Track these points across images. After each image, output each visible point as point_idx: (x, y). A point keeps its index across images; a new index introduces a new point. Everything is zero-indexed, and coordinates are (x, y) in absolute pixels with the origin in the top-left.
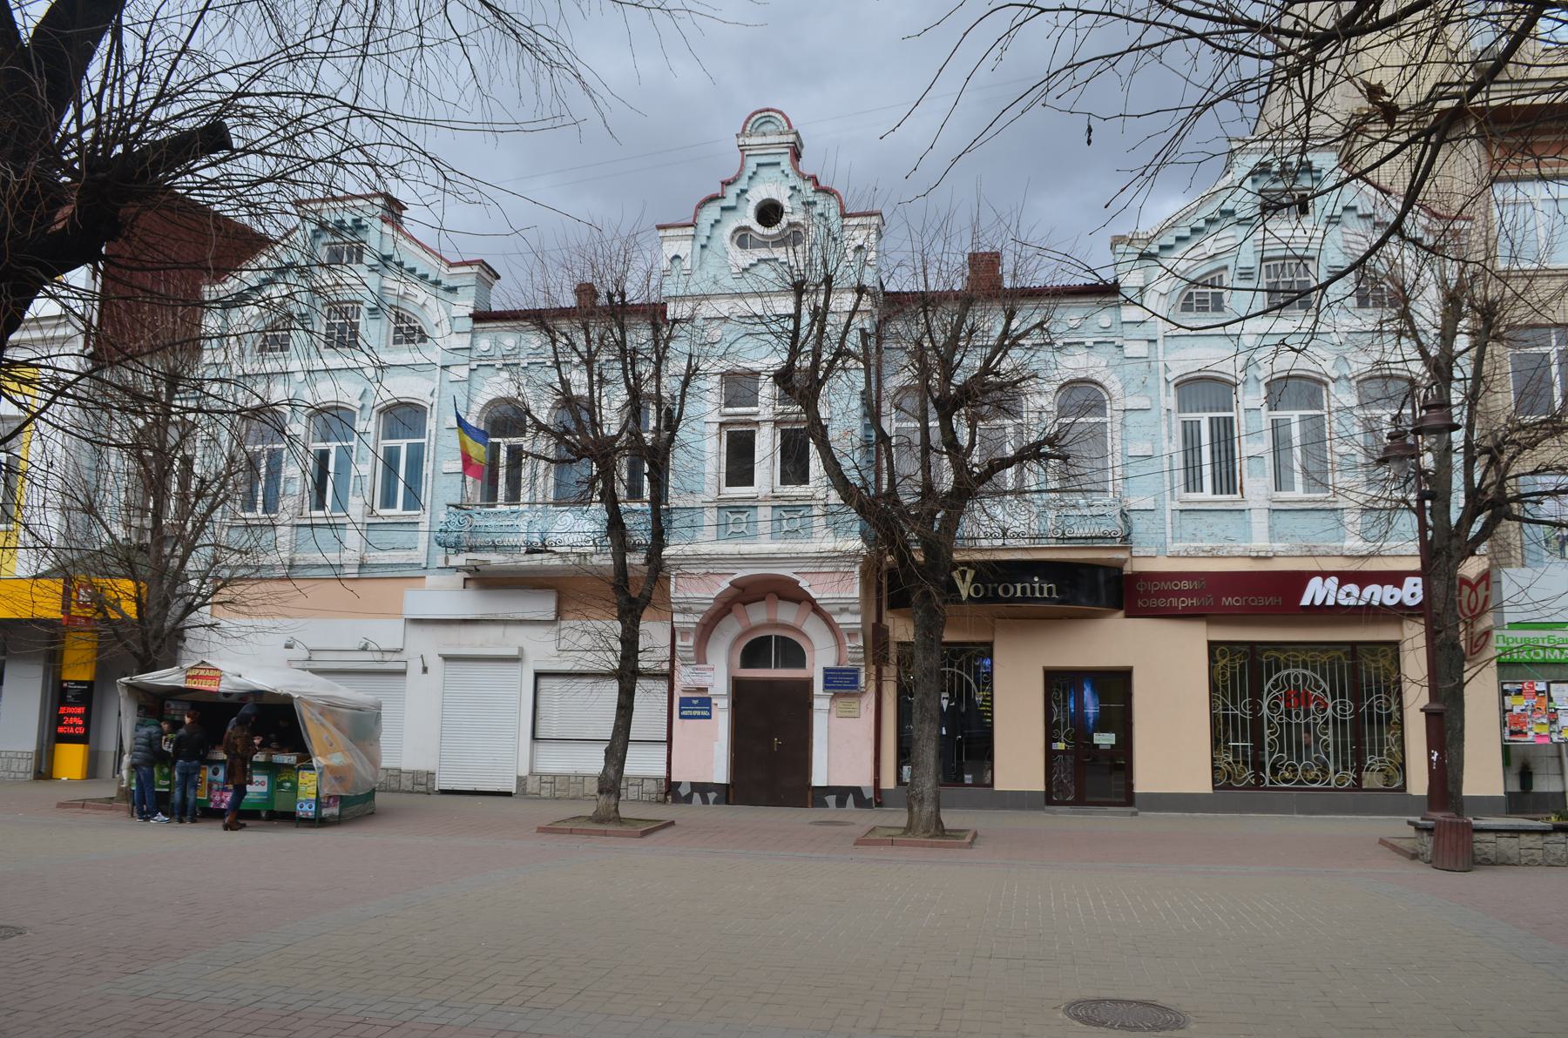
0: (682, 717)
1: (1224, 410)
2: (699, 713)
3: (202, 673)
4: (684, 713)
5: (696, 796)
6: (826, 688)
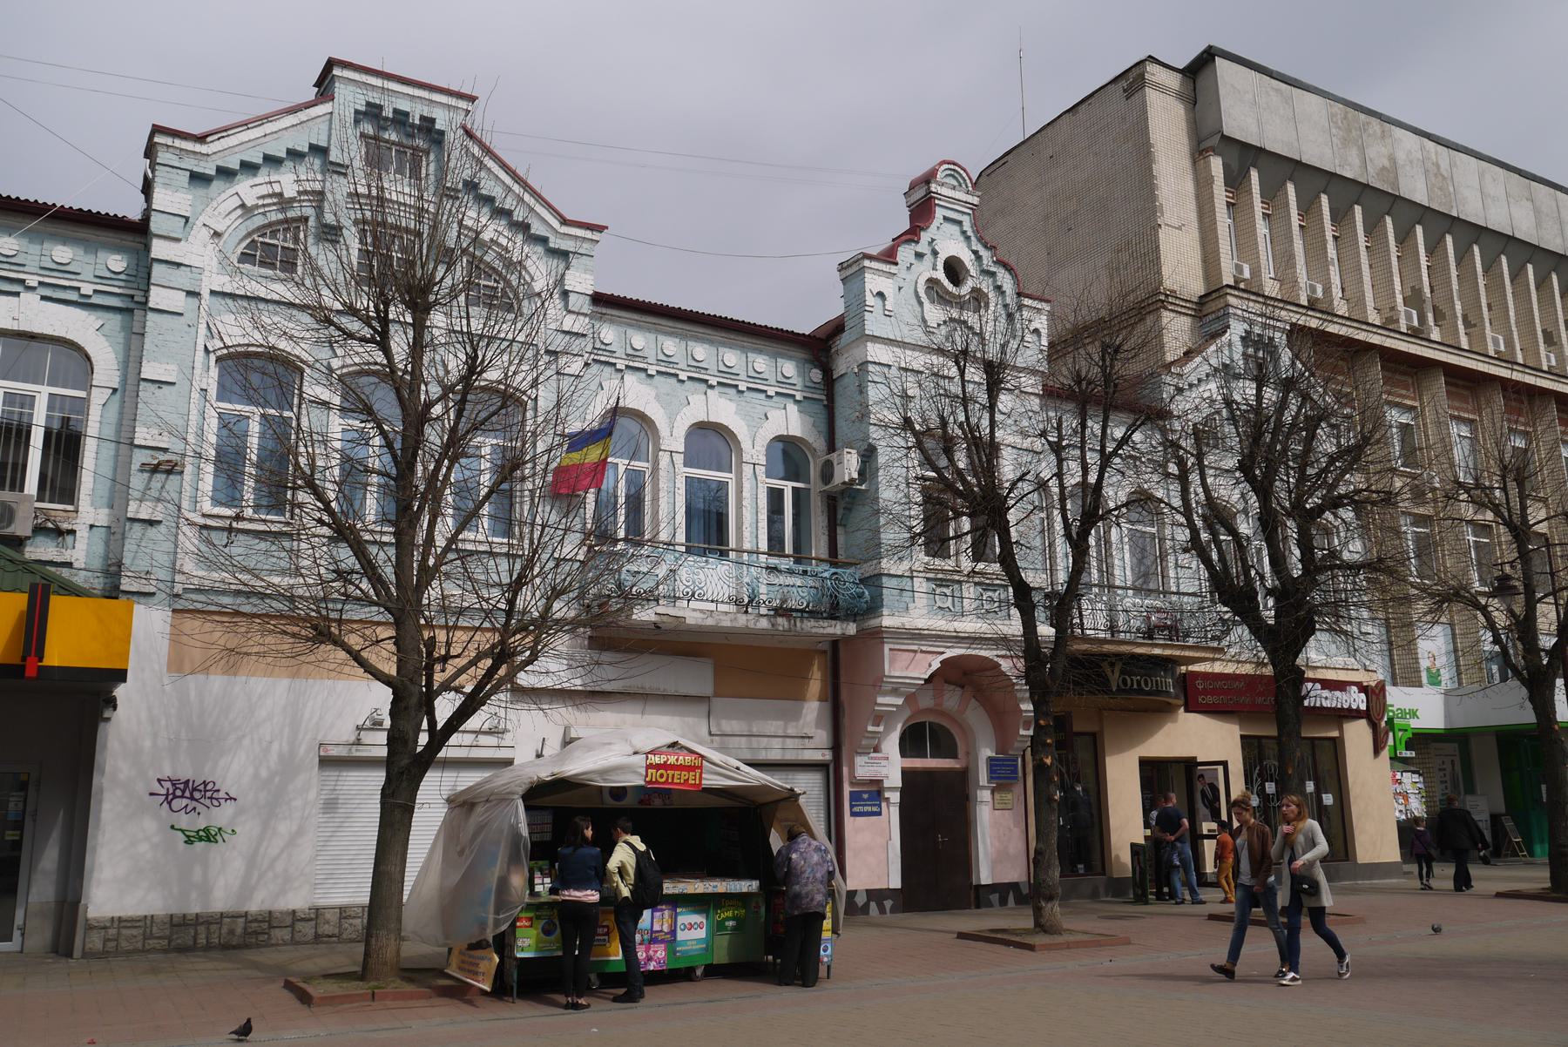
0: (853, 814)
1: (6, 469)
2: (869, 809)
3: (672, 760)
4: (856, 809)
5: (873, 905)
6: (991, 779)
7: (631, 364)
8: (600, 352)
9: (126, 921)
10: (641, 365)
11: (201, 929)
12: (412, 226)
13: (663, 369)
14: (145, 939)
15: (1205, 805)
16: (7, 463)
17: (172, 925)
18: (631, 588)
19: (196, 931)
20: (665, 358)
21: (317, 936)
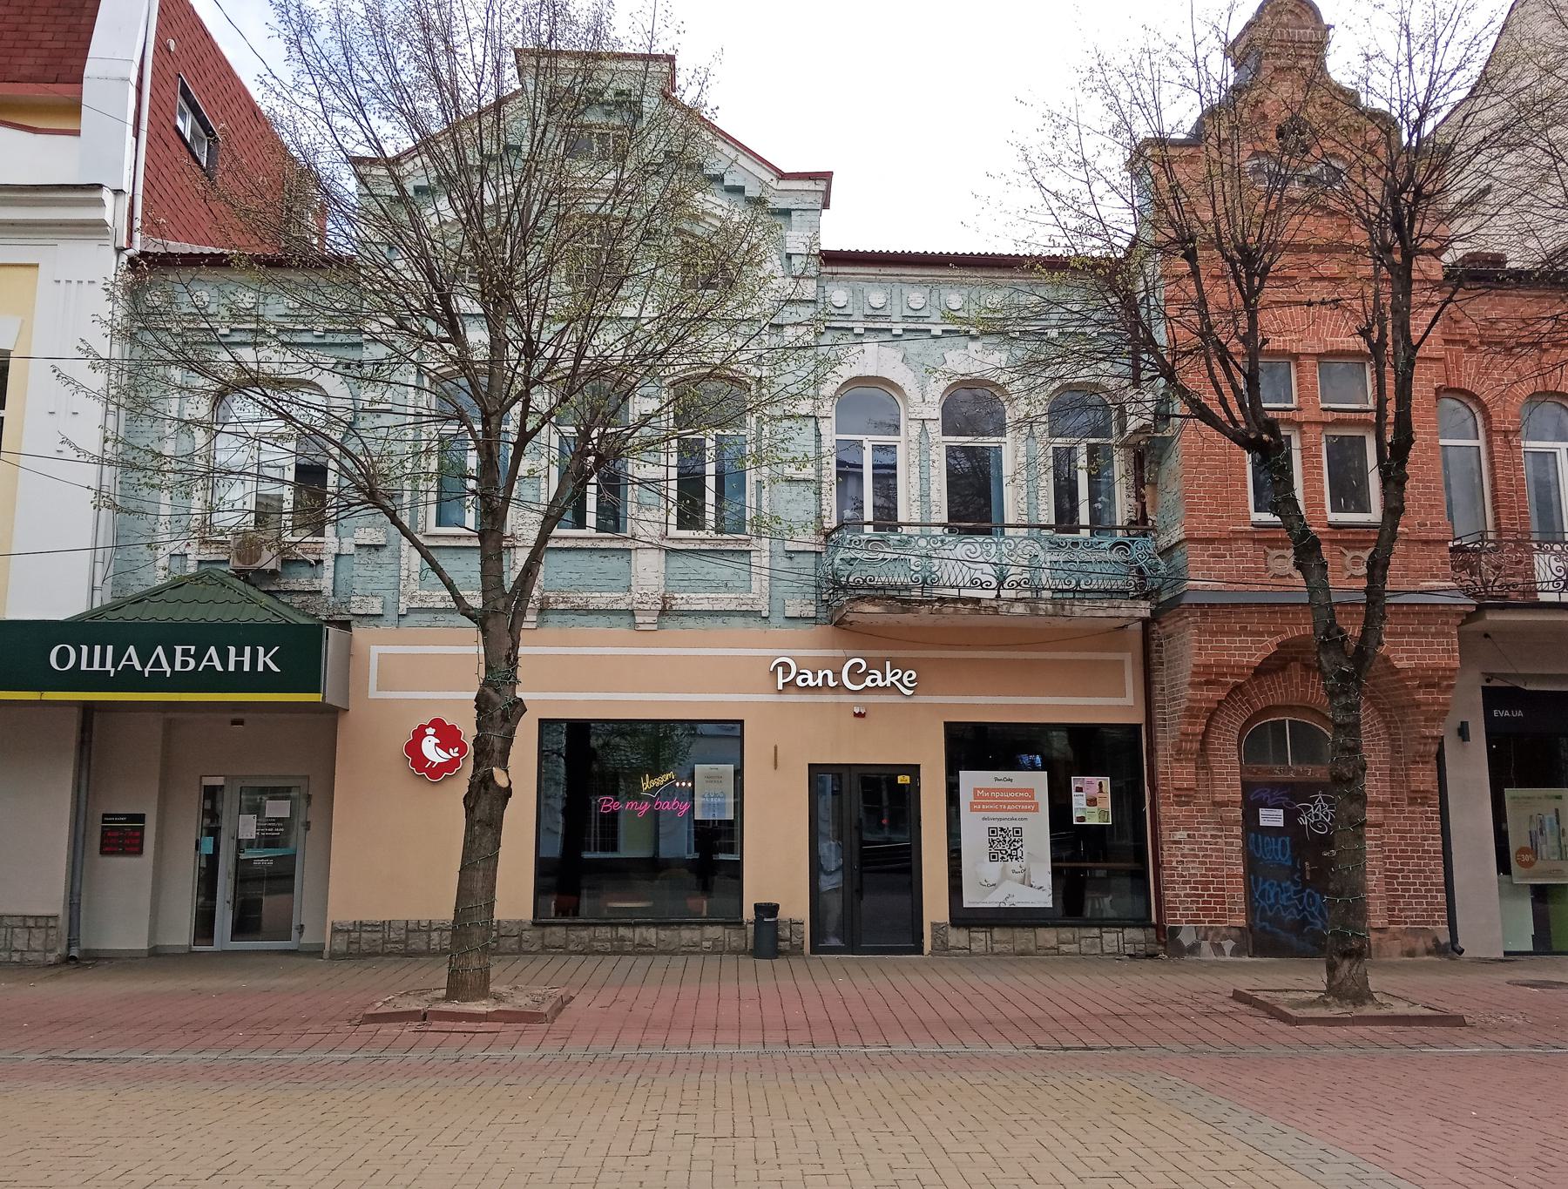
7: (871, 325)
8: (833, 318)
9: (366, 925)
10: (884, 326)
11: (435, 935)
12: (503, 211)
13: (912, 326)
14: (384, 943)
15: (1369, 944)
16: (703, 476)
17: (408, 931)
18: (848, 579)
19: (429, 936)
20: (911, 313)
21: (544, 947)
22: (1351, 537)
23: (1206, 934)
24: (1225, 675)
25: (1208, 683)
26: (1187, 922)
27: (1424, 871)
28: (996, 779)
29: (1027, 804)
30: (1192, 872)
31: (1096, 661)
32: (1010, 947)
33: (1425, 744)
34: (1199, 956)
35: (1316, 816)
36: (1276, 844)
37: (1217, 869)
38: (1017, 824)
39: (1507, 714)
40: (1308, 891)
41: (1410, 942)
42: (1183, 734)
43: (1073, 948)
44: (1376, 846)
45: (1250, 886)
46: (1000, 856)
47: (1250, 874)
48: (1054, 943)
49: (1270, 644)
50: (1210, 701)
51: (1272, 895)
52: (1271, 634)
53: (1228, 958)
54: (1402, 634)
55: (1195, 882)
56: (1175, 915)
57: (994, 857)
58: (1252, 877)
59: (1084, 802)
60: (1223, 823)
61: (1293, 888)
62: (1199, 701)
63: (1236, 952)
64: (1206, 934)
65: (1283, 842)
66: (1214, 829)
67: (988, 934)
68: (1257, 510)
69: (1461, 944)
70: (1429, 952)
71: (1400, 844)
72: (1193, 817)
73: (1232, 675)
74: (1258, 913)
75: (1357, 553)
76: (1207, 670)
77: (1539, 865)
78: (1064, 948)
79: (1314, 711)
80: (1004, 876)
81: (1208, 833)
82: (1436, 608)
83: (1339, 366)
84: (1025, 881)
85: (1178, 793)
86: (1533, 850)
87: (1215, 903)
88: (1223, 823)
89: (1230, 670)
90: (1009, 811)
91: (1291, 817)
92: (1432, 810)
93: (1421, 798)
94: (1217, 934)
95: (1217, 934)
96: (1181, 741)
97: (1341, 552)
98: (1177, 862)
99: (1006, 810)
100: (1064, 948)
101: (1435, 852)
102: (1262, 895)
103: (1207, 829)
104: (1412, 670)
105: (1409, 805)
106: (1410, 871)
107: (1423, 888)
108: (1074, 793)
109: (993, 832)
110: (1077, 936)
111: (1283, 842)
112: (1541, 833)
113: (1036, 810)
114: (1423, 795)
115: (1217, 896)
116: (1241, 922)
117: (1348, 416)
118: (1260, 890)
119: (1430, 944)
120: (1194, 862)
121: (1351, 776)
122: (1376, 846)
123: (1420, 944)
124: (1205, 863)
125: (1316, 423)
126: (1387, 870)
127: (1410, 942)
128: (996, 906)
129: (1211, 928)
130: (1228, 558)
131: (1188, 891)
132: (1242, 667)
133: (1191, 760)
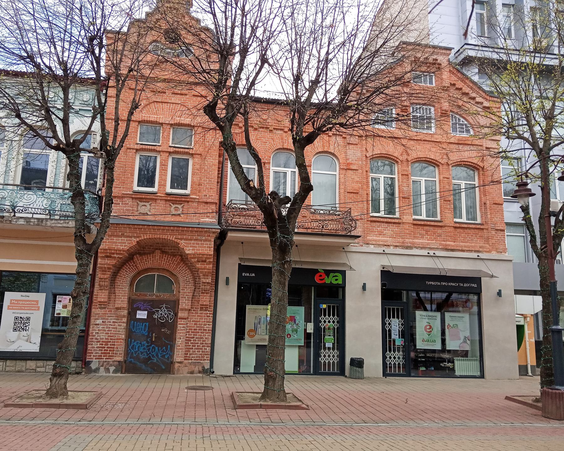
22: (174, 199)
23: (103, 364)
24: (114, 254)
25: (107, 257)
26: (96, 359)
27: (203, 338)
28: (22, 296)
29: (35, 307)
30: (102, 337)
31: (13, 243)
32: (13, 368)
33: (205, 286)
34: (98, 373)
35: (161, 314)
36: (142, 326)
37: (113, 336)
38: (28, 316)
39: (248, 275)
40: (153, 345)
41: (193, 368)
42: (100, 278)
43: (43, 369)
44: (183, 327)
45: (128, 343)
46: (18, 329)
47: (129, 338)
48: (34, 367)
49: (134, 241)
50: (109, 265)
51: (137, 347)
52: (134, 237)
53: (111, 374)
54: (191, 240)
55: (103, 342)
56: (91, 356)
57: (15, 329)
58: (129, 339)
59: (61, 307)
60: (119, 317)
61: (146, 344)
62: (105, 264)
63: (115, 372)
64: (103, 364)
65: (145, 325)
66: (114, 319)
67: (4, 363)
68: (138, 186)
69: (215, 369)
70: (200, 372)
71: (194, 327)
72: (105, 314)
73: (117, 254)
74: (129, 356)
75: (177, 206)
76: (105, 251)
77: (257, 337)
78: (38, 369)
79: (168, 271)
80: (19, 338)
81: (112, 321)
82: (194, 229)
83: (182, 130)
84: (28, 340)
85: (100, 303)
86: (255, 330)
87: (110, 351)
88: (119, 317)
89: (115, 252)
90: (26, 310)
91: (150, 314)
92: (210, 313)
93: (205, 308)
94: (108, 364)
95: (108, 364)
96: (100, 281)
97: (170, 205)
98: (96, 333)
99: (24, 309)
100: (38, 369)
101: (209, 330)
102: (132, 348)
103: (112, 319)
104: (194, 254)
105: (201, 310)
106: (197, 338)
107: (201, 345)
108: (57, 303)
109: (28, 319)
110: (45, 364)
111: (145, 325)
112: (259, 324)
113: (38, 310)
114: (205, 307)
115: (111, 348)
116: (120, 359)
117: (179, 150)
118: (132, 344)
119: (201, 369)
120: (103, 333)
121: (75, 295)
122: (183, 327)
123: (196, 369)
124: (108, 333)
125: (166, 152)
126: (187, 337)
127: (193, 368)
128: (13, 351)
129: (106, 361)
130: (121, 205)
131: (98, 345)
132: (120, 251)
133: (107, 290)
